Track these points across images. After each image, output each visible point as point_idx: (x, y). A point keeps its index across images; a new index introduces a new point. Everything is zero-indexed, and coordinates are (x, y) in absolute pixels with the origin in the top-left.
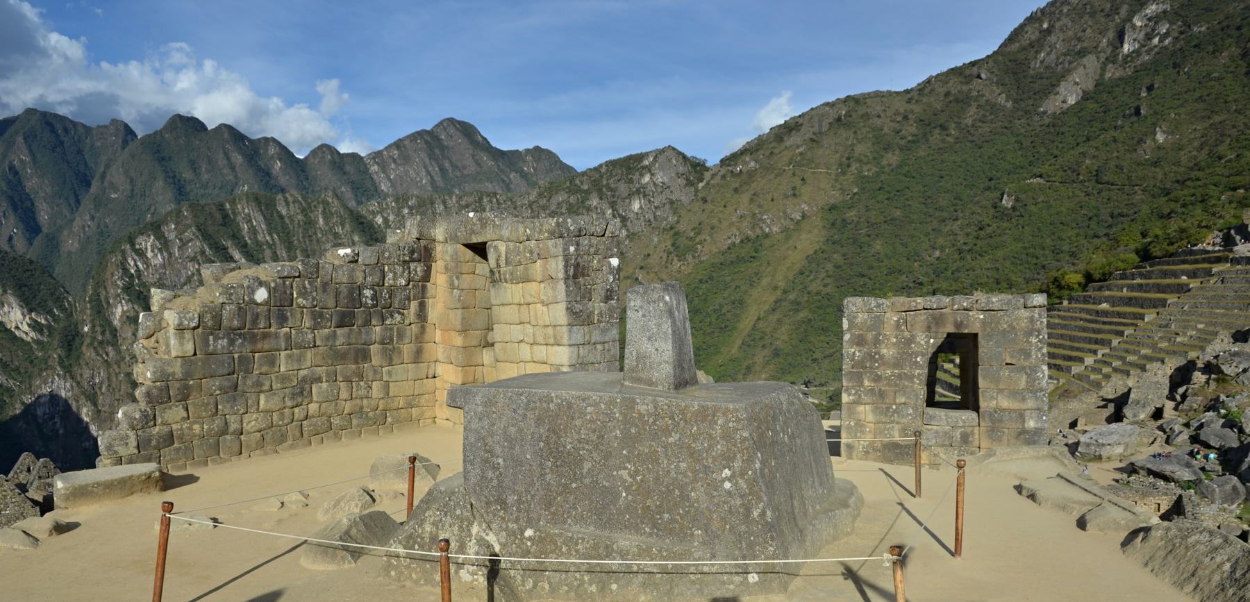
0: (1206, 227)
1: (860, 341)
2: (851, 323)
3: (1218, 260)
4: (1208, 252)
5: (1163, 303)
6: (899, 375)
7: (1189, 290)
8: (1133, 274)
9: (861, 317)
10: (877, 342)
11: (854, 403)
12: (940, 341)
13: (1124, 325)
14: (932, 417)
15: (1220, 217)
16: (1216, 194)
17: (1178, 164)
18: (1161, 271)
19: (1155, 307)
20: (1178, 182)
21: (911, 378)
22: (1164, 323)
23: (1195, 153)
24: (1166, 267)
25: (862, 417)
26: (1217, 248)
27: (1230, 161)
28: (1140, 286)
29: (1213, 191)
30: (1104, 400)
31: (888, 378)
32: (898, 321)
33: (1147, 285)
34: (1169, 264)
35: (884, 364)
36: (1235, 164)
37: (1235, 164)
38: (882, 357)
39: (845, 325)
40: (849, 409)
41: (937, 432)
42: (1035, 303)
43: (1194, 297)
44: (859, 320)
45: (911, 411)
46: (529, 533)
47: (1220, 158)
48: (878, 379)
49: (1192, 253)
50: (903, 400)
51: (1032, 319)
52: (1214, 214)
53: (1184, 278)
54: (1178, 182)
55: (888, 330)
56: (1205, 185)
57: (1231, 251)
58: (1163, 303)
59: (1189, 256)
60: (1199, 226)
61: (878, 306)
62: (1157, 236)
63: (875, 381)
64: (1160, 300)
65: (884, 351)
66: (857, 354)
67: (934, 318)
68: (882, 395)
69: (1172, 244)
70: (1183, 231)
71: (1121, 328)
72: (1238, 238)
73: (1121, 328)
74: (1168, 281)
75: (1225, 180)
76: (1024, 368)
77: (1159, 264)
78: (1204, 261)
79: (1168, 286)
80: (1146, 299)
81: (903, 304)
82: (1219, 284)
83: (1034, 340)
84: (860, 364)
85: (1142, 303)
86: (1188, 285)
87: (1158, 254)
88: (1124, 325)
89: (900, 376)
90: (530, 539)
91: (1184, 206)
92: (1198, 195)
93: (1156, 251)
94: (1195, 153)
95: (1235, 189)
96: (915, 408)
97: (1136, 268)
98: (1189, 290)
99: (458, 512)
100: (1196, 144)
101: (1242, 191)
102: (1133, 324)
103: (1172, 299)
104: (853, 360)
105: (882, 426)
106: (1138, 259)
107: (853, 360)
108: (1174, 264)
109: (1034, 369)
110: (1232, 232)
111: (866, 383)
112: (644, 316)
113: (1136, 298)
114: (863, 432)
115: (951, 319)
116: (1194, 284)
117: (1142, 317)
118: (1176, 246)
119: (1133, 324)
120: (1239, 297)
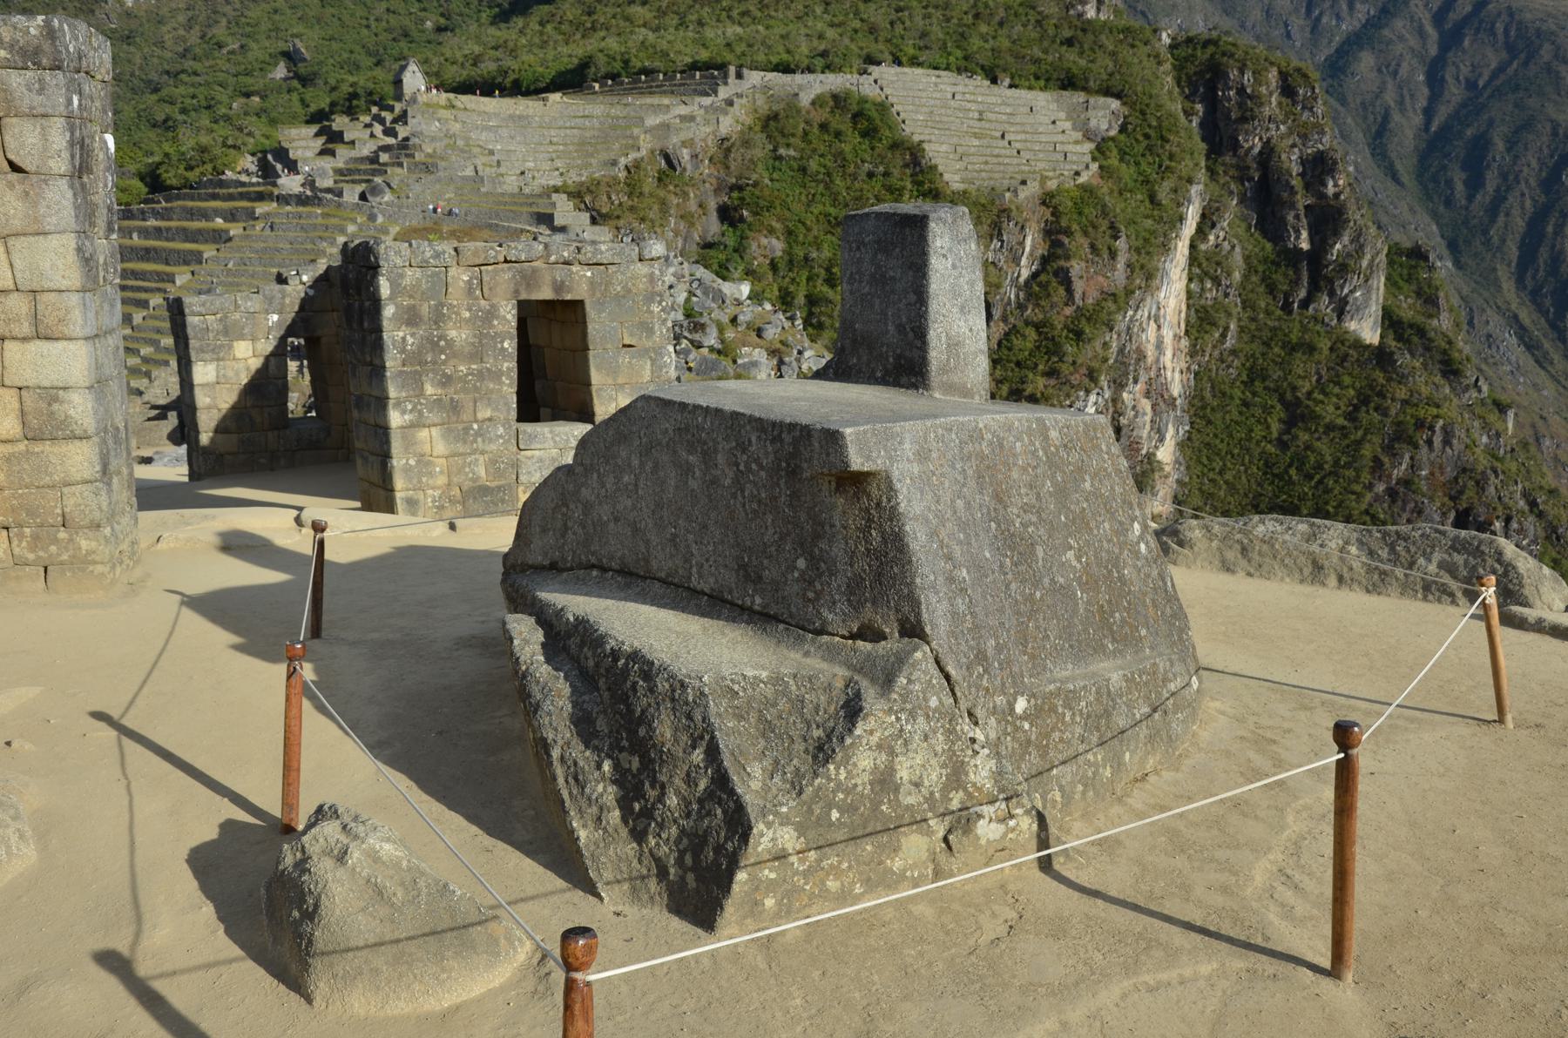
0: (234, 147)
1: (411, 318)
2: (394, 285)
3: (260, 197)
4: (243, 184)
5: (197, 258)
6: (480, 372)
7: (230, 239)
8: (143, 212)
9: (411, 276)
10: (438, 318)
11: (413, 426)
12: (290, 317)
13: (146, 290)
14: (533, 437)
15: (250, 134)
16: (225, 99)
17: (160, 44)
18: (184, 209)
19: (186, 263)
20: (168, 73)
21: (497, 375)
22: (205, 287)
23: (181, 32)
24: (190, 204)
25: (427, 449)
26: (255, 180)
27: (232, 52)
28: (158, 230)
29: (221, 95)
30: (154, 407)
31: (463, 379)
32: (469, 282)
33: (168, 229)
34: (192, 199)
35: (454, 355)
36: (240, 58)
37: (240, 58)
38: (450, 343)
39: (385, 289)
40: (404, 438)
41: (541, 460)
42: (654, 254)
43: (239, 249)
44: (407, 281)
45: (501, 430)
46: (1021, 705)
47: (220, 46)
48: (446, 381)
49: (222, 184)
50: (488, 414)
51: (651, 277)
52: (240, 129)
53: (219, 220)
54: (168, 73)
55: (456, 296)
56: (208, 84)
57: (275, 185)
58: (197, 258)
59: (217, 186)
60: (224, 145)
61: (437, 255)
62: (167, 155)
63: (443, 385)
64: (191, 252)
65: (453, 334)
66: (410, 340)
67: (524, 277)
68: (455, 407)
69: (190, 168)
70: (203, 150)
71: (143, 296)
72: (279, 167)
73: (143, 296)
74: (202, 224)
75: (232, 80)
76: (647, 351)
77: (178, 198)
78: (242, 196)
79: (200, 231)
80: (172, 251)
81: (476, 253)
82: (268, 232)
83: (656, 309)
84: (415, 358)
85: (166, 258)
86: (227, 231)
87: (174, 182)
88: (146, 290)
89: (480, 375)
90: (1026, 716)
91: (184, 111)
92: (201, 97)
93: (170, 177)
94: (181, 32)
95: (248, 95)
96: (506, 423)
97: (146, 201)
98: (230, 239)
99: (934, 702)
100: (181, 18)
101: (257, 99)
102: (159, 290)
103: (209, 251)
104: (403, 351)
105: (459, 460)
106: (145, 190)
107: (403, 351)
108: (200, 199)
109: (659, 351)
110: (270, 157)
111: (429, 389)
112: (954, 267)
113: (155, 249)
114: (431, 475)
115: (548, 278)
116: (235, 230)
117: (171, 279)
118: (197, 171)
119: (159, 290)
120: (297, 250)
